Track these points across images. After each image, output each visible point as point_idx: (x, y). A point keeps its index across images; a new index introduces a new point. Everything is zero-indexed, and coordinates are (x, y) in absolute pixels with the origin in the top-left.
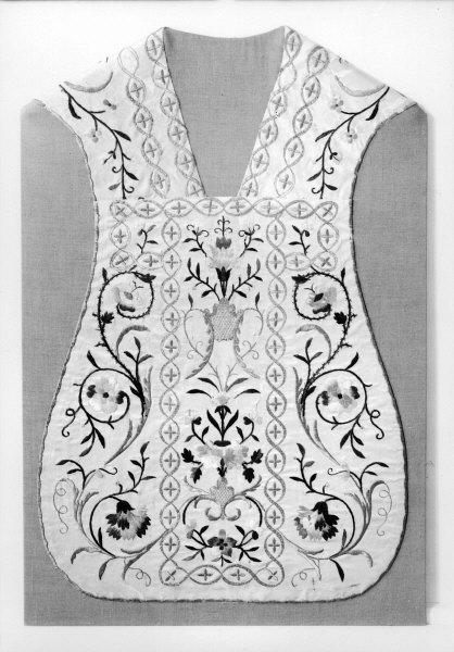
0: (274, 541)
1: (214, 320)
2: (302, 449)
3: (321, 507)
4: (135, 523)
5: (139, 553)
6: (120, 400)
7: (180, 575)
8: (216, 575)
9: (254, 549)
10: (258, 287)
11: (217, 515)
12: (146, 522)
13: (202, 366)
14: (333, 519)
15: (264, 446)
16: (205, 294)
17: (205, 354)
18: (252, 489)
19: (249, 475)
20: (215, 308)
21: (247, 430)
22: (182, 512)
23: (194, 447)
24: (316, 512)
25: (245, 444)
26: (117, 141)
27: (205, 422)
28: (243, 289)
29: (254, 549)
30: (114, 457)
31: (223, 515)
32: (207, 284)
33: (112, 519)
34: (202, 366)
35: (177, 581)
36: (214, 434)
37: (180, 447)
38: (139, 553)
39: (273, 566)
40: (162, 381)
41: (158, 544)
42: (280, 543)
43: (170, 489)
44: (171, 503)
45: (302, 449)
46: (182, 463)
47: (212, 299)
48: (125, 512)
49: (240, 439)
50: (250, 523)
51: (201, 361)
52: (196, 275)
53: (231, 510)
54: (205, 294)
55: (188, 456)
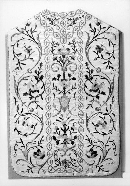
0: (80, 160)
1: (62, 101)
2: (15, 98)
3: (91, 150)
4: (41, 155)
5: (42, 166)
6: (32, 127)
7: (53, 170)
8: (64, 170)
9: (75, 163)
10: (75, 91)
11: (63, 154)
12: (44, 156)
13: (58, 114)
14: (95, 152)
15: (78, 134)
16: (59, 93)
17: (59, 110)
18: (73, 147)
19: (73, 143)
20: (62, 97)
21: (72, 131)
22: (45, 92)
23: (56, 135)
24: (91, 152)
25: (71, 135)
26: (27, 33)
27: (60, 129)
28: (70, 91)
29: (75, 163)
30: (35, 138)
31: (65, 154)
32: (59, 90)
33: (35, 153)
34: (58, 114)
35: (53, 172)
36: (62, 133)
37: (52, 135)
38: (42, 166)
39: (80, 167)
40: (61, 25)
41: (47, 163)
42: (82, 160)
43: (44, 24)
44: (50, 142)
45: (15, 98)
46: (53, 139)
47: (62, 95)
48: (39, 152)
49: (70, 134)
50: (73, 156)
51: (58, 112)
52: (55, 88)
53: (68, 153)
54: (59, 93)
55: (54, 138)
